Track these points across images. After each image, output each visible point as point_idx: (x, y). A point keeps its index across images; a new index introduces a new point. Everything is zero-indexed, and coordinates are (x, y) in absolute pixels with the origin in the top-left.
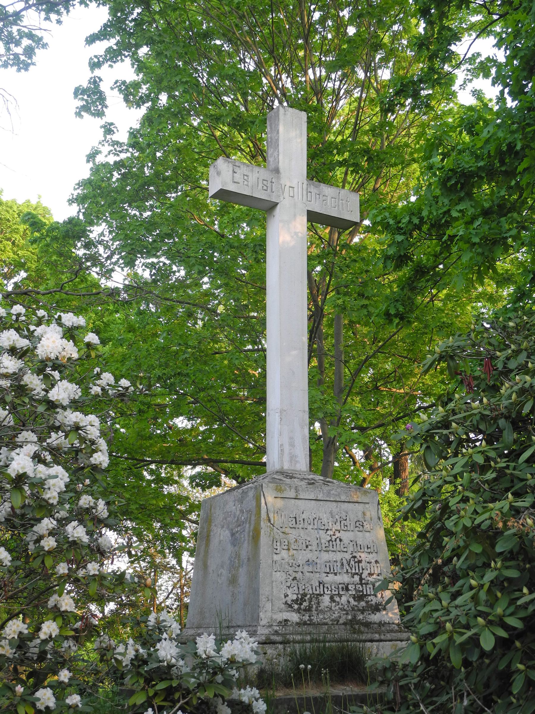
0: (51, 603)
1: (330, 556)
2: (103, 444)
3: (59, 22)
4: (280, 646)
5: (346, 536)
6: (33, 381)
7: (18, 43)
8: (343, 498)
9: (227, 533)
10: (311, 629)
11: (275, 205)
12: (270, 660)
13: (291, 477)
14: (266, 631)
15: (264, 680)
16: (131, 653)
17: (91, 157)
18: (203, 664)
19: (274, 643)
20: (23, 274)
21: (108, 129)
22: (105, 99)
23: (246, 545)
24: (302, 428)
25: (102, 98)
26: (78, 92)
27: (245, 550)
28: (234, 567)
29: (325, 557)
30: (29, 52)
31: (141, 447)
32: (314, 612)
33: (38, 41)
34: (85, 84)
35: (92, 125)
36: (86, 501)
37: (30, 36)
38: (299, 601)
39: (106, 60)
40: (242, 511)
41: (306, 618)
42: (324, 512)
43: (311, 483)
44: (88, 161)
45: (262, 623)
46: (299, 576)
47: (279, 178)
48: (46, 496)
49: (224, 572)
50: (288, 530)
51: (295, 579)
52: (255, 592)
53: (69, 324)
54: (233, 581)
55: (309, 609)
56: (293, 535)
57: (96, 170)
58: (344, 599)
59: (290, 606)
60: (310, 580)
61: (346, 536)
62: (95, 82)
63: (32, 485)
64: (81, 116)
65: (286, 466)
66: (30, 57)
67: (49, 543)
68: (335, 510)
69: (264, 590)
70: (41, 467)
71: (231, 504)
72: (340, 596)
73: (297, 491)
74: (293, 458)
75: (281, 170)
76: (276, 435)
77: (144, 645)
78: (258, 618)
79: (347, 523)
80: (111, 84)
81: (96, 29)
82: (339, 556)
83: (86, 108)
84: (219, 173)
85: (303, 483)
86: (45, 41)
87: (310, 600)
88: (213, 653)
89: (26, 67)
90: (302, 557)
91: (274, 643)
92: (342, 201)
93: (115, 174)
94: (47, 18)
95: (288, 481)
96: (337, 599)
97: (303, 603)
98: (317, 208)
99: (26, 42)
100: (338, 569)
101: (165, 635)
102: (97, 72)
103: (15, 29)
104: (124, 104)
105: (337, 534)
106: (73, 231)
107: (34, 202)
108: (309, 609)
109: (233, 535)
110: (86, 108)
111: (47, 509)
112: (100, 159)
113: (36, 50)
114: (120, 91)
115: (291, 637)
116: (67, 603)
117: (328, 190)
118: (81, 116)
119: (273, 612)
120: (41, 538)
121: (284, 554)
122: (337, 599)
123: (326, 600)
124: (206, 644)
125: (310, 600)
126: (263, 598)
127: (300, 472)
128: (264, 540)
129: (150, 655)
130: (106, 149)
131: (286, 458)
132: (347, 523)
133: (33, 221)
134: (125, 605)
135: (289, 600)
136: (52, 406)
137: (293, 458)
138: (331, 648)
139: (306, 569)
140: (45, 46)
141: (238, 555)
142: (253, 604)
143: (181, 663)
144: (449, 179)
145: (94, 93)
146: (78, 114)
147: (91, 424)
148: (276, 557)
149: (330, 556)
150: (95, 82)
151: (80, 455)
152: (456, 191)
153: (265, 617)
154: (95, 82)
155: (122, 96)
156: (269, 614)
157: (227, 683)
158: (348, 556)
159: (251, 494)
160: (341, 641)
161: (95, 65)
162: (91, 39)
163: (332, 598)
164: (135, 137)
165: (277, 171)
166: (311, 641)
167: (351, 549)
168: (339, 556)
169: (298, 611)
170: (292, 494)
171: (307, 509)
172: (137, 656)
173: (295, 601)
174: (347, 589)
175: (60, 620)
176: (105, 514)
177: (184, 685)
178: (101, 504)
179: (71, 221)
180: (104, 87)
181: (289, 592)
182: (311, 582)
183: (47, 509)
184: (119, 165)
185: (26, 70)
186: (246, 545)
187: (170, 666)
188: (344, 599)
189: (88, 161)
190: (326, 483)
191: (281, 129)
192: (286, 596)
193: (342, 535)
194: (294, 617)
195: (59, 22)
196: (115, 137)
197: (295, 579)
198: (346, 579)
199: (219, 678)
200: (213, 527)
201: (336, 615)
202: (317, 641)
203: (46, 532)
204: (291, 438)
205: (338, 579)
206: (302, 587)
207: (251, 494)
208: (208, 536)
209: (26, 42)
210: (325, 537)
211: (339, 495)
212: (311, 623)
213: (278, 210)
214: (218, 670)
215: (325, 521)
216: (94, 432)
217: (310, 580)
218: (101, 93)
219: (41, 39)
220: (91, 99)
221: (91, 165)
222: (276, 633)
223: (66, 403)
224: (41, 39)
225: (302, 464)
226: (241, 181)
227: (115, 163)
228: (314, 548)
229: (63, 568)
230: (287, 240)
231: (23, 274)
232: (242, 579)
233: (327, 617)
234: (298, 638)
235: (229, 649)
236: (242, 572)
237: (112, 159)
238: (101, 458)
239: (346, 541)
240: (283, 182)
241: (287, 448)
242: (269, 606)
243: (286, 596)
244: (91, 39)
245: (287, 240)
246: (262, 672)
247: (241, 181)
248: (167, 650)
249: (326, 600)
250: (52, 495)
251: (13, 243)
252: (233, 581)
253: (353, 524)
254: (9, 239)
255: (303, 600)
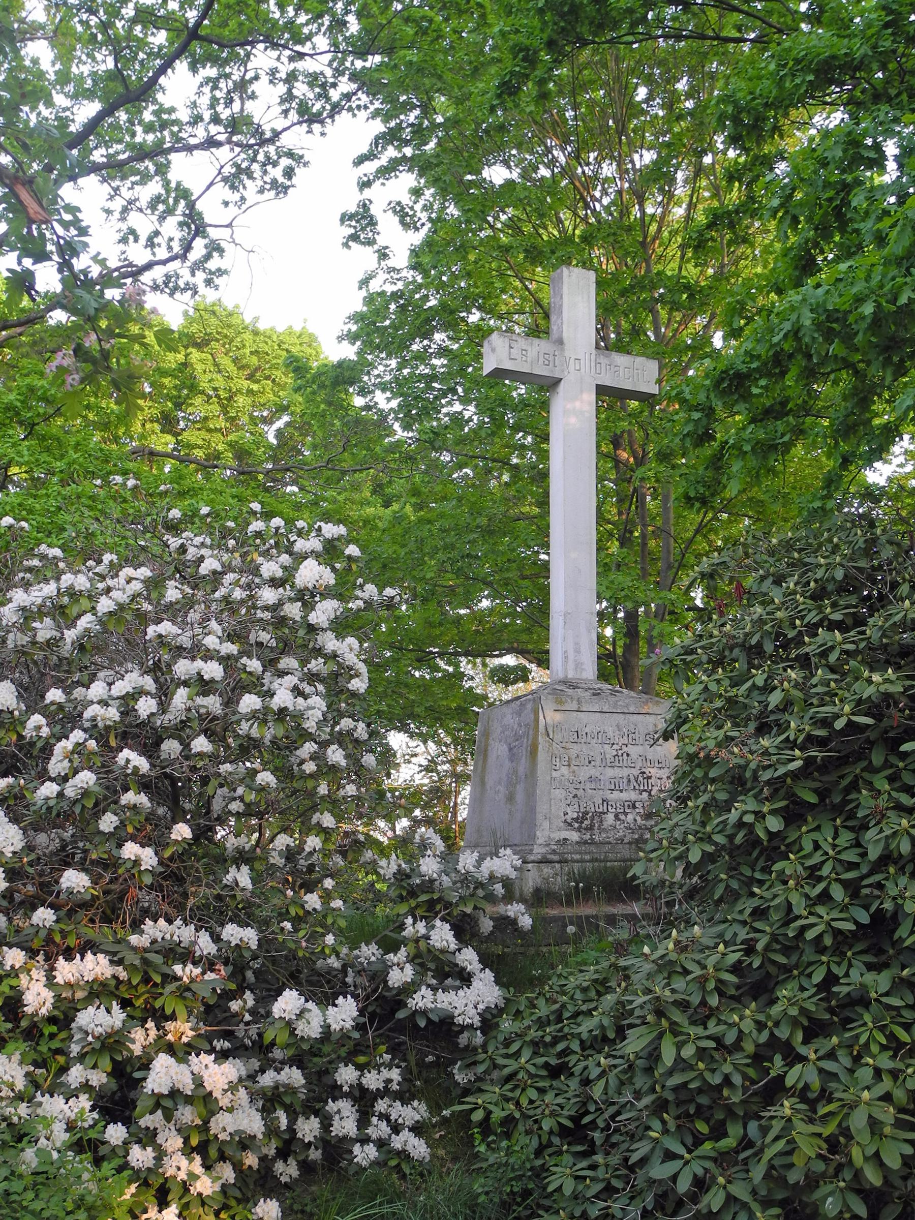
0: (314, 820)
1: (617, 772)
2: (362, 668)
3: (323, 134)
4: (557, 866)
5: (634, 751)
6: (293, 610)
7: (275, 164)
8: (632, 709)
9: (505, 747)
10: (593, 848)
11: (560, 380)
12: (546, 879)
13: (575, 687)
14: (543, 850)
15: (538, 899)
16: (394, 868)
17: (364, 282)
18: (465, 879)
19: (551, 862)
20: (286, 418)
21: (383, 255)
22: (376, 224)
23: (523, 760)
24: (589, 632)
25: (372, 223)
26: (345, 218)
27: (523, 766)
28: (511, 784)
29: (610, 772)
30: (289, 173)
31: (429, 636)
32: (596, 831)
33: (299, 159)
34: (353, 209)
35: (365, 257)
36: (346, 723)
37: (290, 154)
38: (580, 820)
39: (377, 177)
40: (520, 725)
41: (587, 837)
42: (609, 725)
43: (597, 694)
44: (360, 288)
45: (539, 842)
46: (580, 793)
47: (563, 350)
48: (305, 726)
49: (502, 789)
50: (569, 745)
51: (575, 796)
52: (531, 810)
53: (328, 536)
54: (510, 798)
55: (590, 828)
56: (574, 750)
57: (369, 300)
58: (630, 818)
59: (570, 825)
60: (592, 797)
61: (634, 751)
62: (364, 205)
63: (293, 717)
64: (349, 247)
65: (571, 675)
66: (290, 178)
67: (310, 767)
68: (622, 723)
69: (542, 808)
70: (300, 700)
71: (509, 717)
72: (626, 814)
73: (579, 701)
74: (578, 665)
75: (565, 340)
76: (560, 641)
77: (408, 862)
78: (534, 837)
79: (636, 736)
80: (385, 206)
81: (364, 149)
82: (625, 772)
83: (354, 237)
84: (493, 350)
85: (588, 694)
86: (306, 159)
87: (592, 818)
88: (472, 869)
89: (286, 189)
90: (584, 773)
91: (551, 862)
92: (639, 373)
93: (393, 307)
94: (310, 131)
95: (570, 692)
96: (622, 817)
97: (585, 821)
98: (608, 381)
99: (285, 162)
100: (624, 786)
101: (429, 852)
102: (368, 193)
103: (271, 149)
104: (400, 227)
105: (625, 749)
106: (344, 376)
107: (297, 328)
108: (590, 828)
109: (510, 749)
110: (354, 237)
111: (306, 736)
112: (375, 286)
113: (297, 170)
114: (395, 212)
115: (569, 857)
116: (328, 820)
117: (621, 360)
118: (349, 247)
119: (551, 830)
120: (302, 762)
121: (565, 770)
122: (622, 817)
123: (610, 818)
124: (467, 861)
125: (592, 818)
126: (540, 817)
127: (586, 681)
128: (542, 756)
129: (412, 870)
130: (382, 276)
131: (571, 665)
132: (636, 736)
133: (297, 366)
134: (420, 821)
135: (569, 818)
136: (312, 629)
137: (578, 665)
138: (613, 868)
139: (588, 785)
140: (306, 164)
141: (515, 772)
142: (529, 822)
143: (445, 878)
144: (723, 379)
145: (363, 217)
146: (346, 245)
147: (349, 649)
148: (554, 774)
149: (617, 772)
150: (365, 206)
151: (340, 679)
152: (732, 393)
153: (542, 836)
154: (365, 206)
155: (397, 219)
156: (547, 833)
157: (491, 898)
158: (636, 772)
159: (529, 706)
160: (624, 861)
161: (365, 185)
162: (360, 161)
163: (617, 817)
164: (417, 256)
165: (560, 342)
166: (592, 861)
167: (639, 764)
168: (625, 772)
169: (579, 830)
170: (574, 706)
171: (590, 722)
172: (400, 871)
173: (576, 820)
174: (634, 807)
175: (322, 836)
176: (365, 736)
177: (447, 898)
178: (361, 725)
179: (341, 364)
180: (375, 210)
181: (569, 810)
182: (593, 800)
183: (306, 736)
184: (395, 296)
185: (286, 193)
186: (523, 760)
187: (432, 881)
188: (630, 818)
189: (360, 288)
190: (613, 693)
191: (565, 290)
192: (566, 814)
193: (631, 750)
194: (574, 836)
195: (323, 134)
196: (390, 263)
197: (575, 796)
198: (633, 796)
199: (481, 893)
200: (491, 742)
201: (621, 834)
202: (596, 860)
203: (307, 756)
204: (576, 644)
205: (624, 796)
206: (583, 804)
207: (529, 706)
208: (486, 751)
209: (285, 162)
210: (610, 752)
211: (627, 706)
212: (593, 842)
213: (562, 387)
214: (479, 885)
215: (610, 734)
216: (351, 659)
217: (592, 797)
218: (372, 217)
219: (302, 157)
220: (361, 223)
221: (364, 293)
222: (554, 852)
223: (325, 625)
224: (302, 157)
225: (590, 671)
226: (518, 357)
227: (393, 293)
228: (598, 763)
229: (323, 790)
230: (573, 423)
231: (286, 418)
232: (520, 797)
233: (612, 836)
234: (578, 857)
235: (489, 865)
236: (520, 789)
237: (390, 289)
238: (359, 685)
239: (634, 756)
240: (567, 354)
241: (571, 656)
242: (546, 824)
243: (566, 814)
244: (360, 161)
245: (573, 423)
246: (537, 891)
247: (518, 357)
248: (429, 866)
249: (610, 818)
250: (310, 725)
251: (274, 381)
252: (510, 798)
253: (642, 737)
254: (267, 378)
255: (584, 818)
